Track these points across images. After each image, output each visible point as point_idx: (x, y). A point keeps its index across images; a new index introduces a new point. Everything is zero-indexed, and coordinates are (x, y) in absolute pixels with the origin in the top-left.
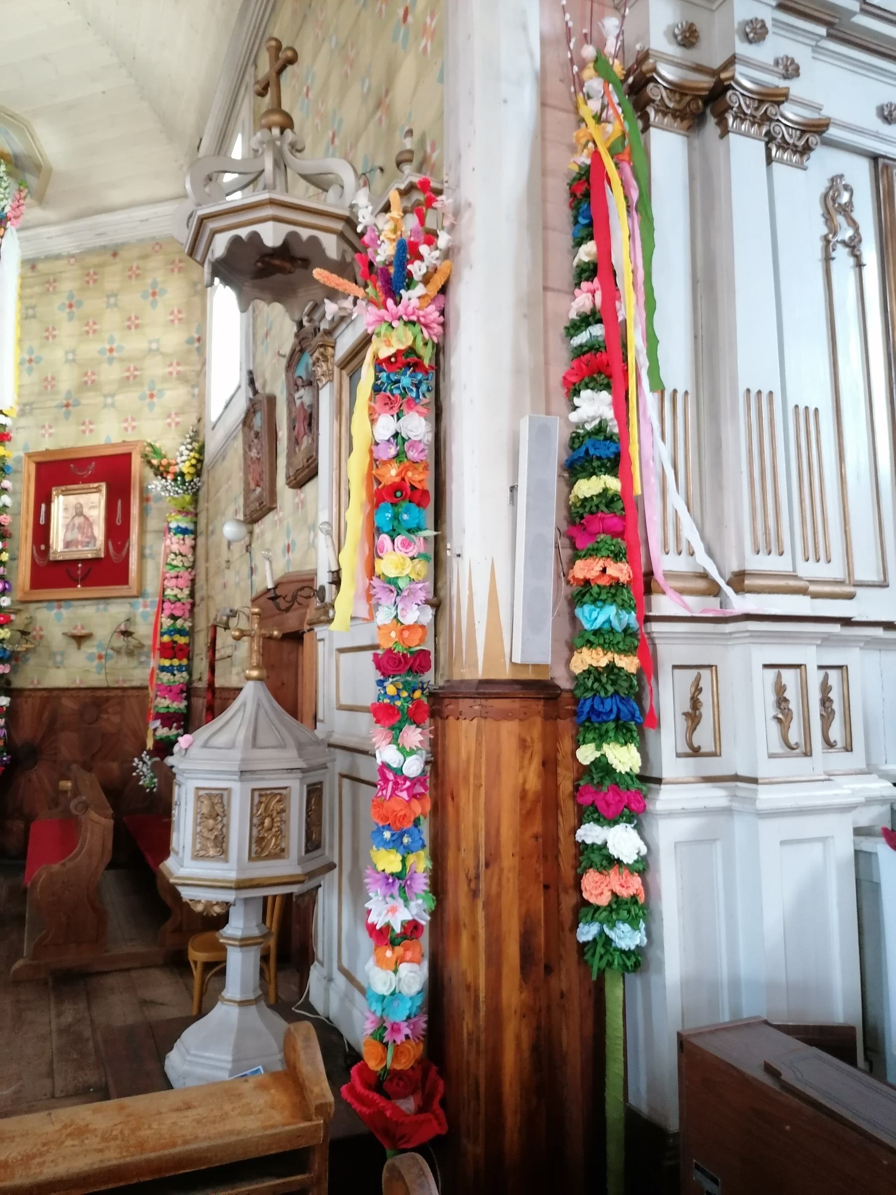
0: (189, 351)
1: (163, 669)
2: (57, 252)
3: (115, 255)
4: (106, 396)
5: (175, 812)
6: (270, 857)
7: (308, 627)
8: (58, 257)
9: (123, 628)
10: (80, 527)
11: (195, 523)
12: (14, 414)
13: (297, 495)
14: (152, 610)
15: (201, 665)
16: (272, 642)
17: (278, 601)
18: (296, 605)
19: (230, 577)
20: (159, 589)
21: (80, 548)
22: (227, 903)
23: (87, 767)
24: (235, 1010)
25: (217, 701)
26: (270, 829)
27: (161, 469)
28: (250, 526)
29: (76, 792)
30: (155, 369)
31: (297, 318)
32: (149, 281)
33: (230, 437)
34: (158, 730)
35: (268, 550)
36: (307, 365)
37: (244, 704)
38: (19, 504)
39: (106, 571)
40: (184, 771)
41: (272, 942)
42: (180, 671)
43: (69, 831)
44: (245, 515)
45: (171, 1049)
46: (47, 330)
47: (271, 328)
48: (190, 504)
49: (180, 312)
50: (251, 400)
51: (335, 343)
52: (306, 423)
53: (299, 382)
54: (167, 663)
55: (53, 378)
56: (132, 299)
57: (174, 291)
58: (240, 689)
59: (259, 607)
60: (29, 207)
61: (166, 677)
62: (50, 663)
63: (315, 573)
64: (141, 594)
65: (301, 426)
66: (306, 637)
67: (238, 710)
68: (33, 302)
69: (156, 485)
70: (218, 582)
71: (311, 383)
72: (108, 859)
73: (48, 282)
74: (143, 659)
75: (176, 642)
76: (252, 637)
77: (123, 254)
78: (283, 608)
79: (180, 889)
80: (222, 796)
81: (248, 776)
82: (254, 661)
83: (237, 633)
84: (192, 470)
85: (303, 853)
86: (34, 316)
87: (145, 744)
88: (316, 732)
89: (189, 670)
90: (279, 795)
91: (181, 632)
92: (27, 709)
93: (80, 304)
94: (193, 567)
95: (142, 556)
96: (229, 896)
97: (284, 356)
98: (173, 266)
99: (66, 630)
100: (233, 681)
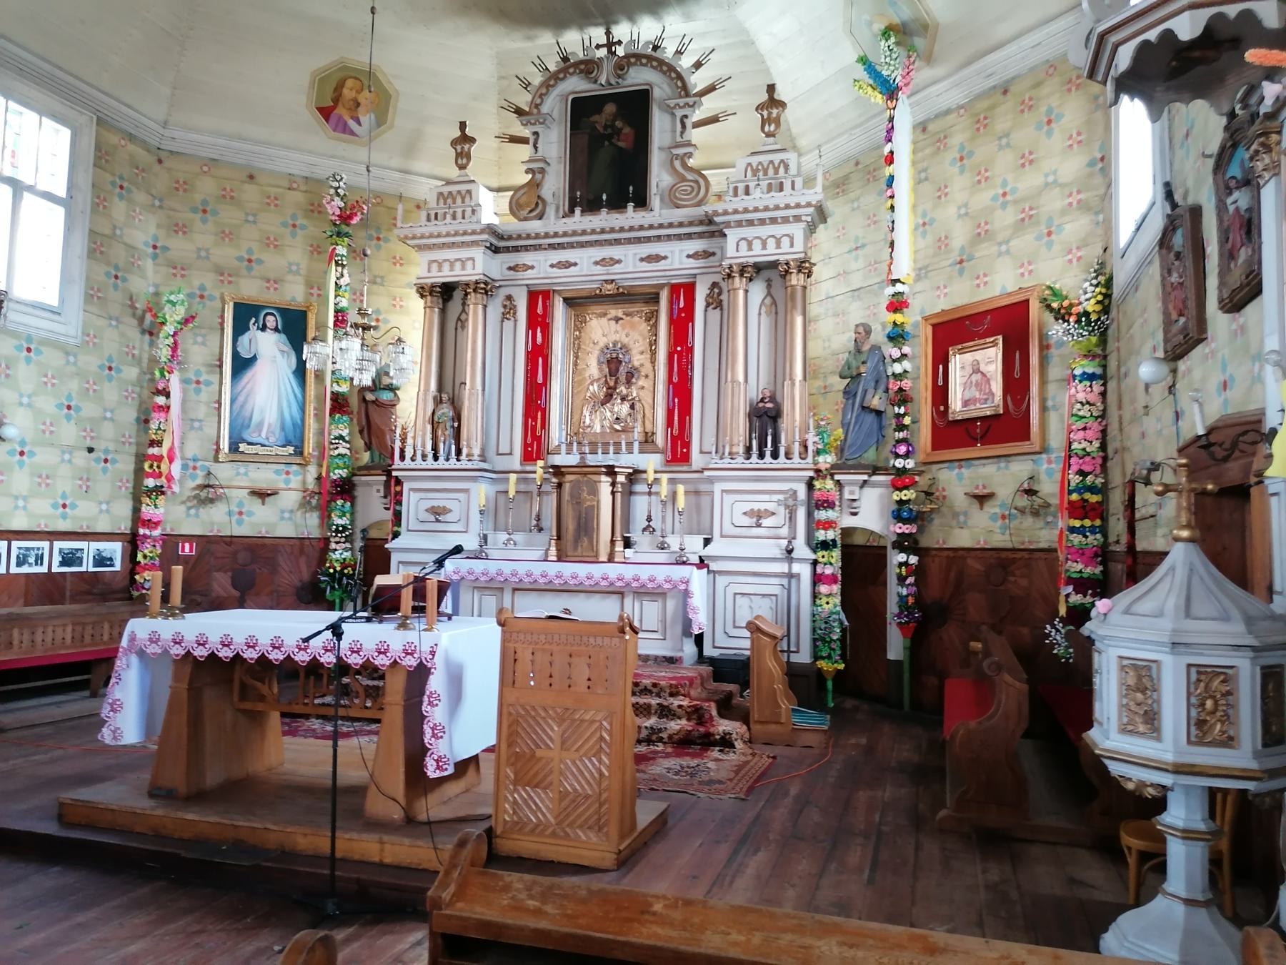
0: (1091, 175)
1: (1072, 530)
2: (945, 108)
3: (1005, 92)
4: (1000, 244)
5: (1096, 680)
6: (1213, 744)
7: (1256, 480)
8: (948, 112)
9: (1026, 486)
10: (977, 384)
11: (1105, 367)
12: (910, 281)
13: (1235, 319)
14: (1057, 467)
15: (1118, 526)
16: (1208, 500)
17: (1212, 449)
18: (1237, 453)
19: (1150, 424)
20: (1065, 444)
21: (978, 405)
22: (1164, 787)
23: (997, 628)
24: (1180, 909)
25: (1139, 565)
26: (1213, 713)
27: (1063, 311)
28: (1172, 364)
29: (987, 653)
30: (1054, 203)
31: (1226, 109)
32: (1044, 109)
33: (1144, 264)
34: (1069, 597)
35: (1196, 390)
36: (1242, 161)
37: (1173, 569)
38: (918, 368)
39: (1006, 427)
40: (1104, 637)
41: (1224, 845)
42: (1093, 533)
43: (984, 689)
44: (1166, 352)
45: (1106, 930)
46: (939, 190)
47: (1192, 127)
48: (1097, 345)
49: (1079, 134)
50: (1168, 216)
51: (1282, 127)
52: (1243, 232)
53: (1233, 184)
54: (1077, 523)
55: (946, 237)
56: (1025, 135)
57: (1073, 111)
58: (1166, 554)
59: (1186, 457)
60: (918, 70)
61: (1077, 539)
62: (954, 523)
63: (1262, 412)
64: (1044, 450)
65: (1236, 236)
66: (1254, 491)
67: (1166, 575)
68: (925, 164)
69: (1056, 330)
70: (1133, 432)
71: (1250, 182)
72: (1024, 726)
73: (939, 141)
74: (1050, 519)
75: (1087, 501)
76: (1180, 492)
77: (1014, 89)
78: (1220, 457)
79: (1107, 762)
80: (1149, 668)
81: (1182, 649)
82: (1184, 520)
83: (1160, 488)
84: (1098, 308)
85: (1260, 747)
86: (926, 179)
87: (1058, 612)
88: (1272, 606)
89: (1104, 531)
90: (1226, 675)
91: (1092, 489)
92: (934, 567)
93: (971, 153)
94: (1103, 415)
95: (1044, 409)
96: (1167, 779)
97: (1210, 156)
98: (1070, 85)
99: (968, 491)
100: (1159, 544)
